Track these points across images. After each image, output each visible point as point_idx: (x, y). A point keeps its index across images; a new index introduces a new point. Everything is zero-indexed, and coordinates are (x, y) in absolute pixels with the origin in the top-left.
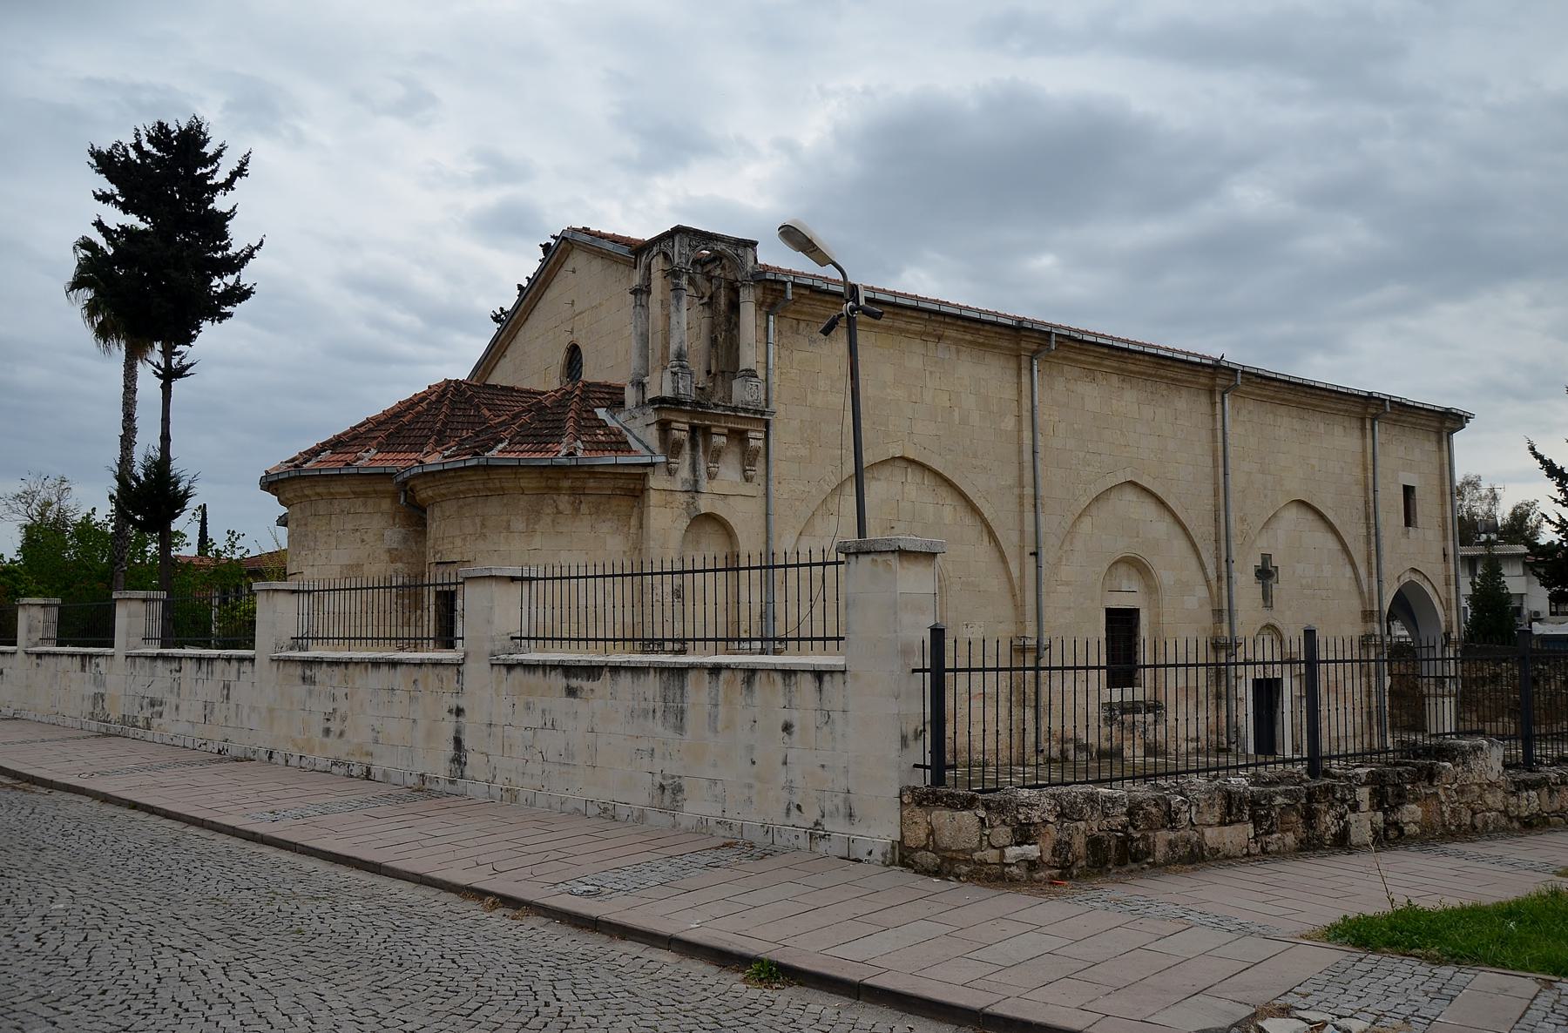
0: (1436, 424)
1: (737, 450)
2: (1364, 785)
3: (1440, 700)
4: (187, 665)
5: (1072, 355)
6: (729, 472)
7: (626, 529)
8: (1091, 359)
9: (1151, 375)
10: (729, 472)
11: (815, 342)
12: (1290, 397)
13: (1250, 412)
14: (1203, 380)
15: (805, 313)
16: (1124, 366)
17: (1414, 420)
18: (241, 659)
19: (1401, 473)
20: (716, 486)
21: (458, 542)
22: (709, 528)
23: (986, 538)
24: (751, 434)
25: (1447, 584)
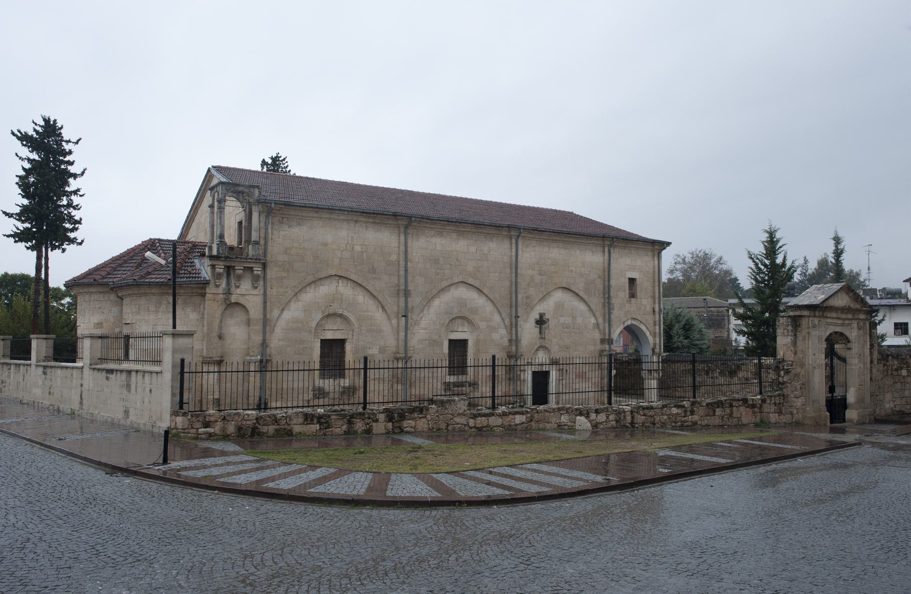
0: (651, 248)
1: (250, 275)
2: (381, 413)
3: (650, 381)
4: (22, 367)
5: (428, 225)
6: (246, 285)
7: (198, 310)
8: (439, 227)
9: (474, 232)
10: (246, 285)
11: (291, 226)
12: (558, 238)
13: (534, 247)
14: (504, 233)
15: (286, 214)
16: (458, 229)
17: (636, 246)
18: (27, 365)
19: (627, 272)
20: (238, 291)
21: (130, 316)
22: (237, 309)
23: (380, 310)
24: (254, 269)
25: (655, 325)
